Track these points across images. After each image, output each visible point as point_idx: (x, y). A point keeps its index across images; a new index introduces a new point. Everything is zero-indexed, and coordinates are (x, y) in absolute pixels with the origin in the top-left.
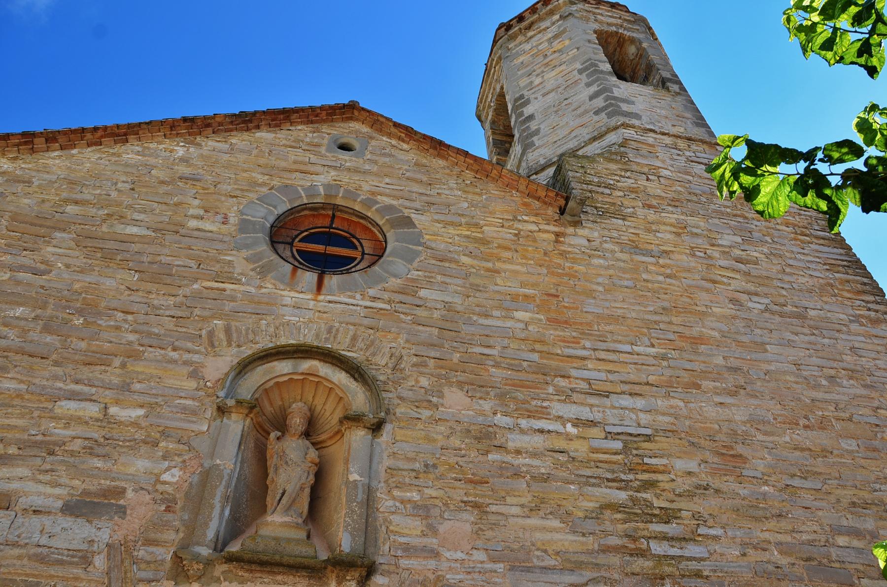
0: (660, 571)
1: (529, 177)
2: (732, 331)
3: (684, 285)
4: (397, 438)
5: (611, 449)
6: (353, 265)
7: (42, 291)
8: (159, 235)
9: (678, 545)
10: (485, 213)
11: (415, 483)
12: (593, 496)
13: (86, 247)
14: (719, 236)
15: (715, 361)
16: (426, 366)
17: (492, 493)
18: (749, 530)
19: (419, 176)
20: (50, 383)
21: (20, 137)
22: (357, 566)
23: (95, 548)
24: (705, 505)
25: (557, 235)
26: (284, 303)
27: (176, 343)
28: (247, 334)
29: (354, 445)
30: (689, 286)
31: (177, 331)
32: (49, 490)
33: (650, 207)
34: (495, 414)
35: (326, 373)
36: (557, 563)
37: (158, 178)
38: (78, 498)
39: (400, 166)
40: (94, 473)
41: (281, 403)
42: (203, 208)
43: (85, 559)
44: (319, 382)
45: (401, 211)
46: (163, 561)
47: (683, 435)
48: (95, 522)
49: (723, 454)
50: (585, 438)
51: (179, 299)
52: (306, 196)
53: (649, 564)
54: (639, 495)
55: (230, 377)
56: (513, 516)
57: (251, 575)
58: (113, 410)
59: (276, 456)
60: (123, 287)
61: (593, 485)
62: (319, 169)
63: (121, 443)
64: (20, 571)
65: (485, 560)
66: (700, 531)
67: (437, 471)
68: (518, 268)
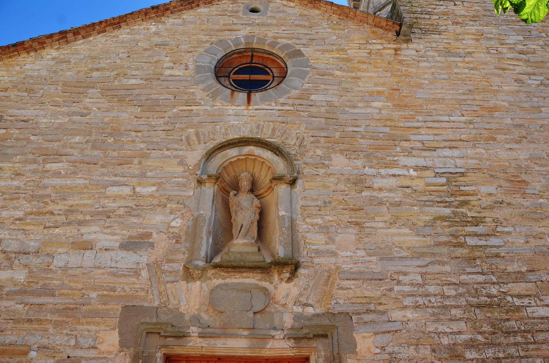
0: (473, 255)
1: (375, 14)
2: (517, 101)
3: (483, 74)
4: (306, 188)
5: (439, 183)
6: (268, 85)
7: (88, 125)
8: (148, 82)
9: (484, 238)
10: (348, 41)
13: (107, 96)
14: (507, 38)
15: (505, 122)
16: (319, 142)
18: (531, 227)
19: (303, 23)
20: (101, 178)
21: (58, 35)
23: (141, 267)
24: (500, 213)
25: (396, 50)
26: (229, 113)
27: (168, 146)
28: (209, 135)
29: (280, 194)
30: (486, 74)
31: (167, 139)
32: (111, 237)
33: (457, 23)
34: (364, 167)
36: (408, 254)
37: (142, 47)
41: (234, 174)
42: (172, 62)
43: (137, 273)
44: (255, 159)
45: (294, 47)
47: (485, 171)
48: (138, 252)
49: (512, 181)
50: (422, 178)
51: (166, 119)
53: (465, 251)
54: (458, 210)
56: (380, 228)
58: (138, 189)
59: (235, 205)
60: (133, 117)
61: (429, 206)
62: (240, 27)
63: (145, 208)
64: (104, 281)
65: (365, 255)
66: (498, 230)
67: (332, 205)
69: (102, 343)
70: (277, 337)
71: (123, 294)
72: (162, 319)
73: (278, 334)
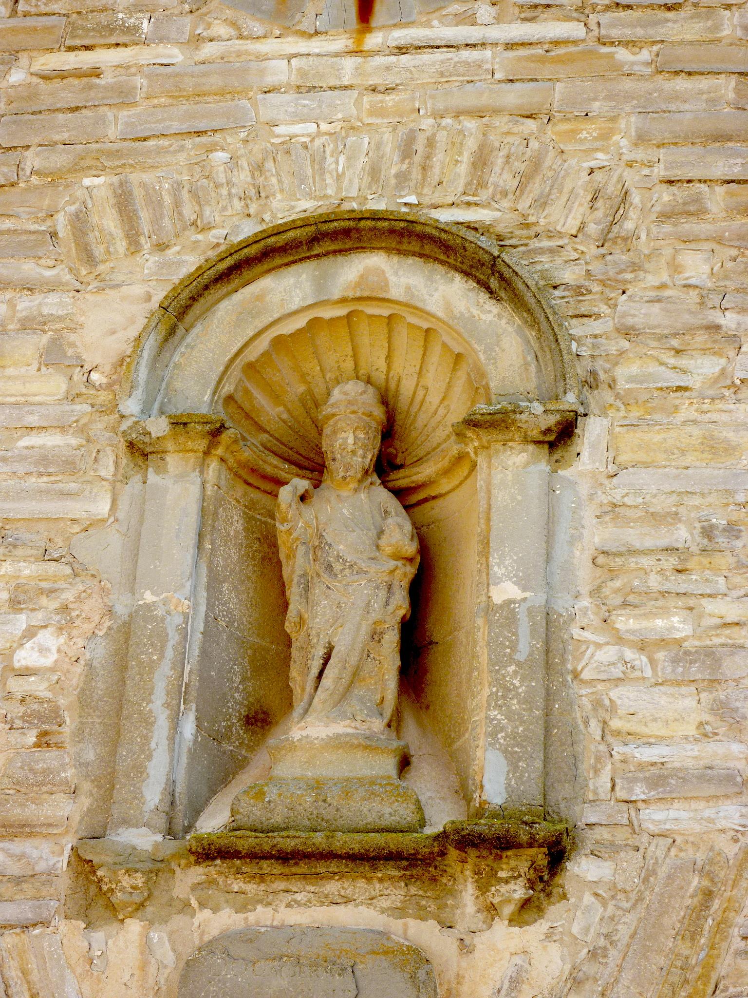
22: (519, 846)
26: (270, 80)
28: (178, 204)
29: (501, 498)
35: (408, 288)
41: (302, 388)
46: (51, 873)
55: (145, 354)
57: (263, 887)
59: (301, 549)
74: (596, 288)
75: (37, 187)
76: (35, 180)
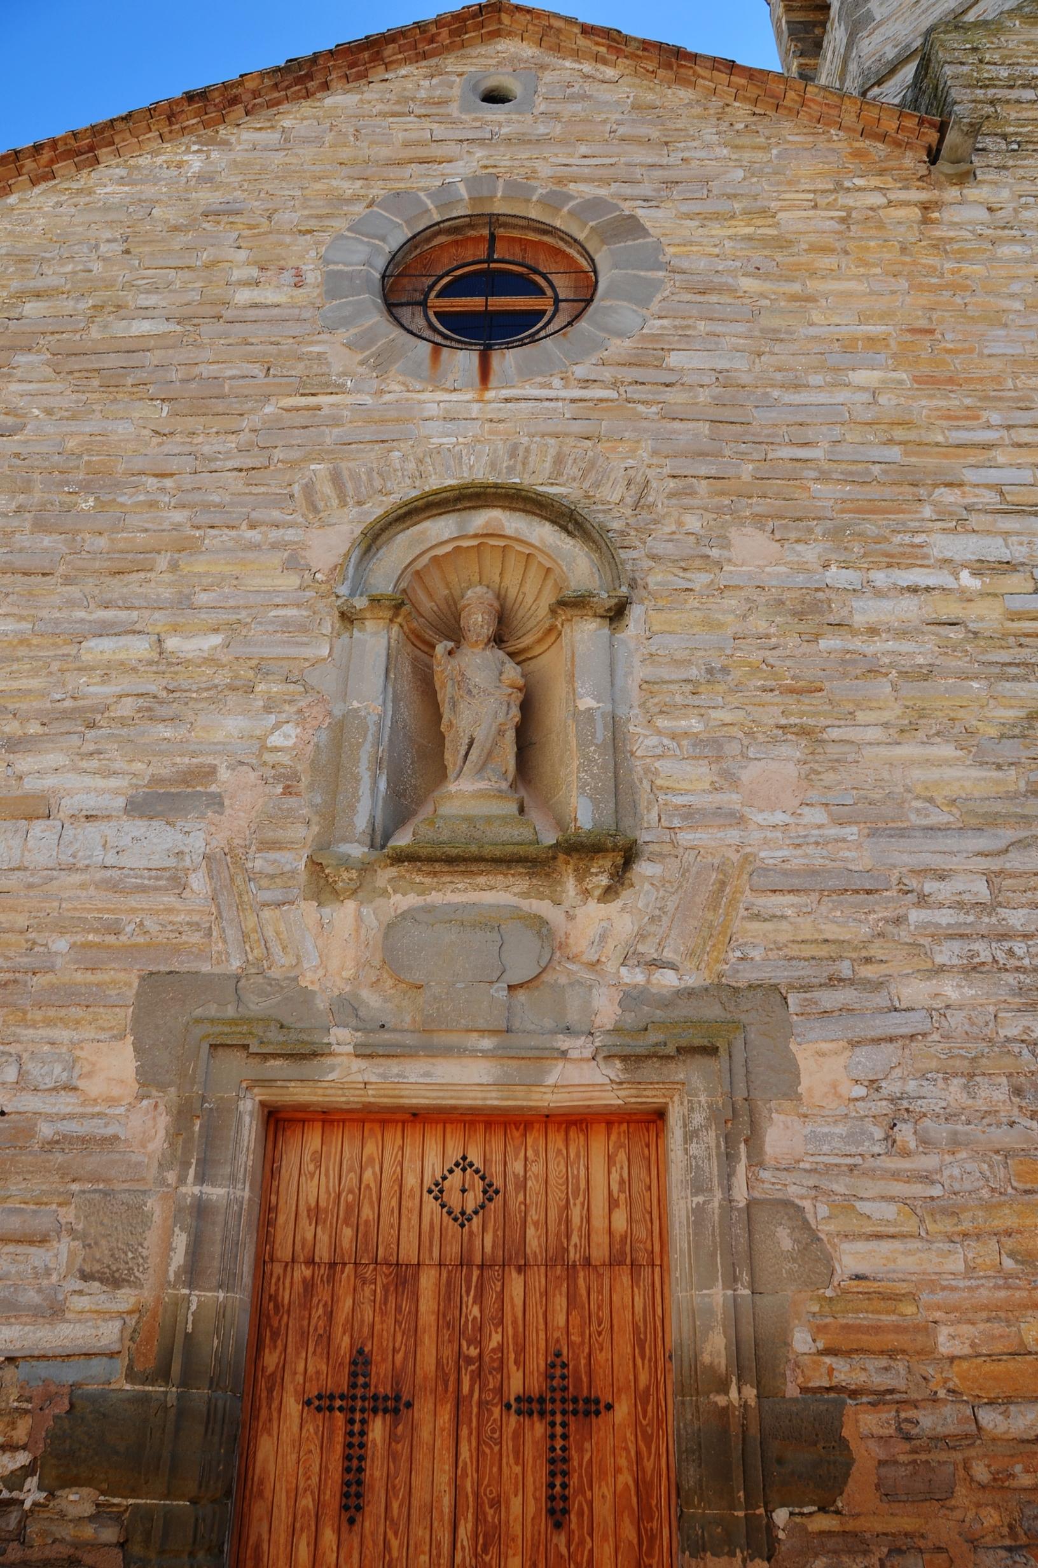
1: (864, 94)
4: (653, 629)
6: (540, 325)
7: (19, 462)
8: (188, 328)
10: (779, 184)
11: (691, 703)
12: (1015, 697)
13: (71, 372)
16: (693, 494)
17: (830, 708)
19: (643, 131)
20: (64, 614)
22: (607, 851)
23: (187, 863)
25: (926, 207)
26: (426, 414)
27: (254, 515)
28: (370, 480)
29: (581, 649)
31: (250, 494)
32: (100, 783)
34: (826, 566)
35: (516, 529)
36: (952, 819)
37: (166, 221)
38: (147, 790)
39: (604, 116)
40: (162, 747)
41: (446, 592)
42: (255, 263)
43: (177, 882)
45: (616, 207)
46: (294, 872)
48: (180, 823)
50: (996, 595)
51: (244, 437)
52: (437, 207)
55: (353, 560)
56: (870, 744)
57: (435, 880)
59: (450, 683)
60: (147, 432)
61: (1015, 678)
62: (452, 149)
63: (194, 695)
64: (88, 906)
67: (730, 678)
68: (851, 285)
69: (89, 1075)
70: (574, 1054)
71: (141, 940)
72: (252, 1006)
73: (579, 1047)
74: (633, 533)
75: (280, 469)
76: (280, 465)
